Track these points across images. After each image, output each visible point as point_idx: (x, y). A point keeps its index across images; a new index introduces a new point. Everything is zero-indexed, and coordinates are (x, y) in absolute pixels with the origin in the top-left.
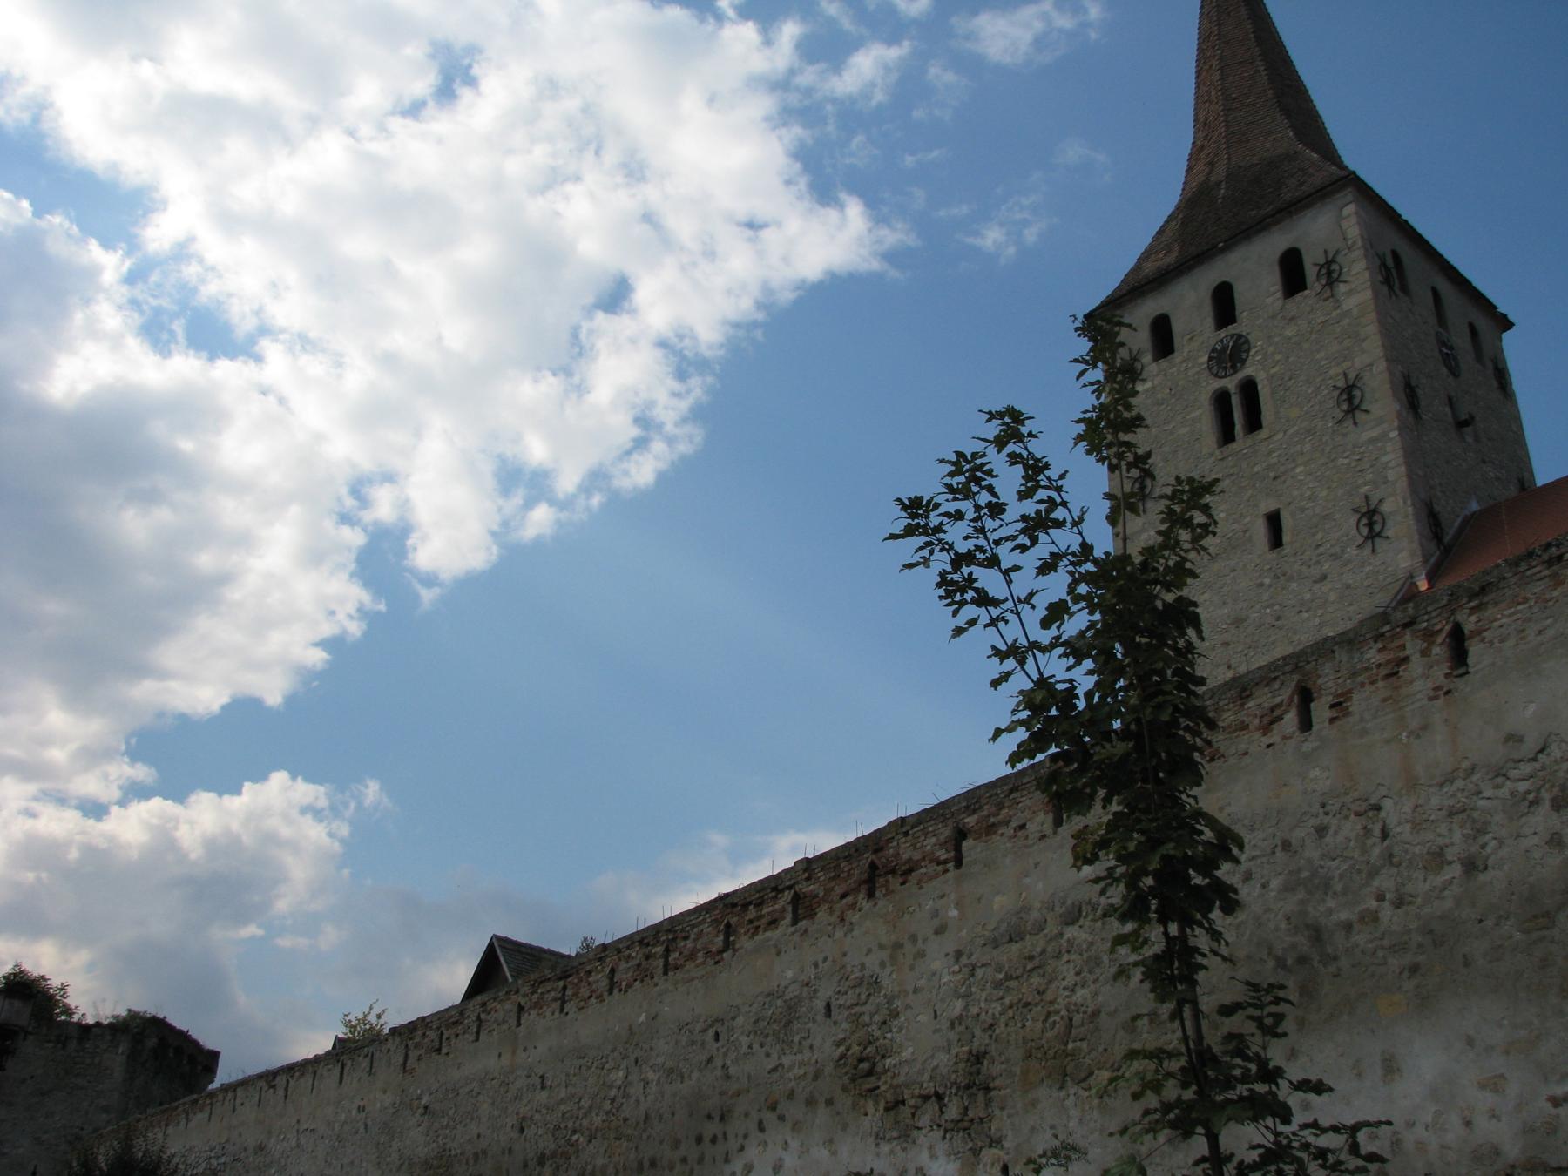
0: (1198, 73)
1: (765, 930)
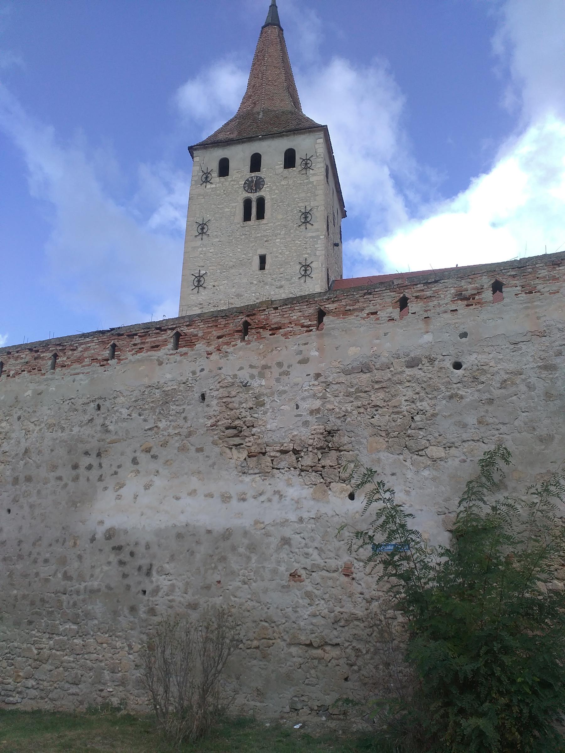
0: (254, 65)
1: (148, 351)
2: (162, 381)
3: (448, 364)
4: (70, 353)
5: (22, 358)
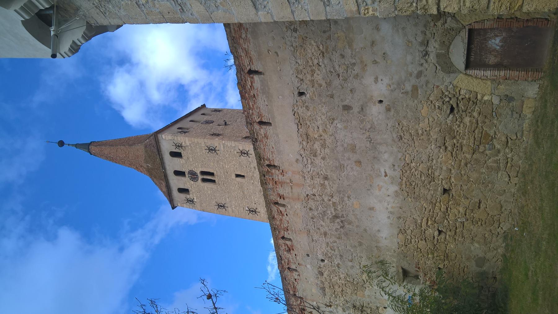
0: (116, 162)
3: (322, 264)
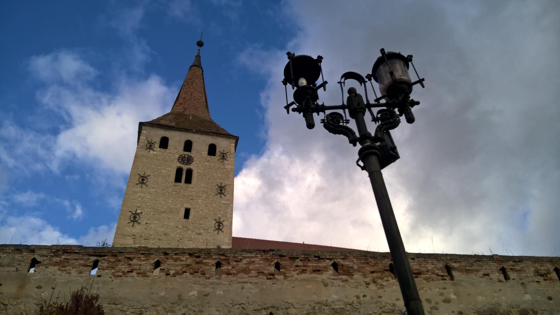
1: (311, 273)
2: (330, 300)
4: (235, 263)
5: (182, 261)
